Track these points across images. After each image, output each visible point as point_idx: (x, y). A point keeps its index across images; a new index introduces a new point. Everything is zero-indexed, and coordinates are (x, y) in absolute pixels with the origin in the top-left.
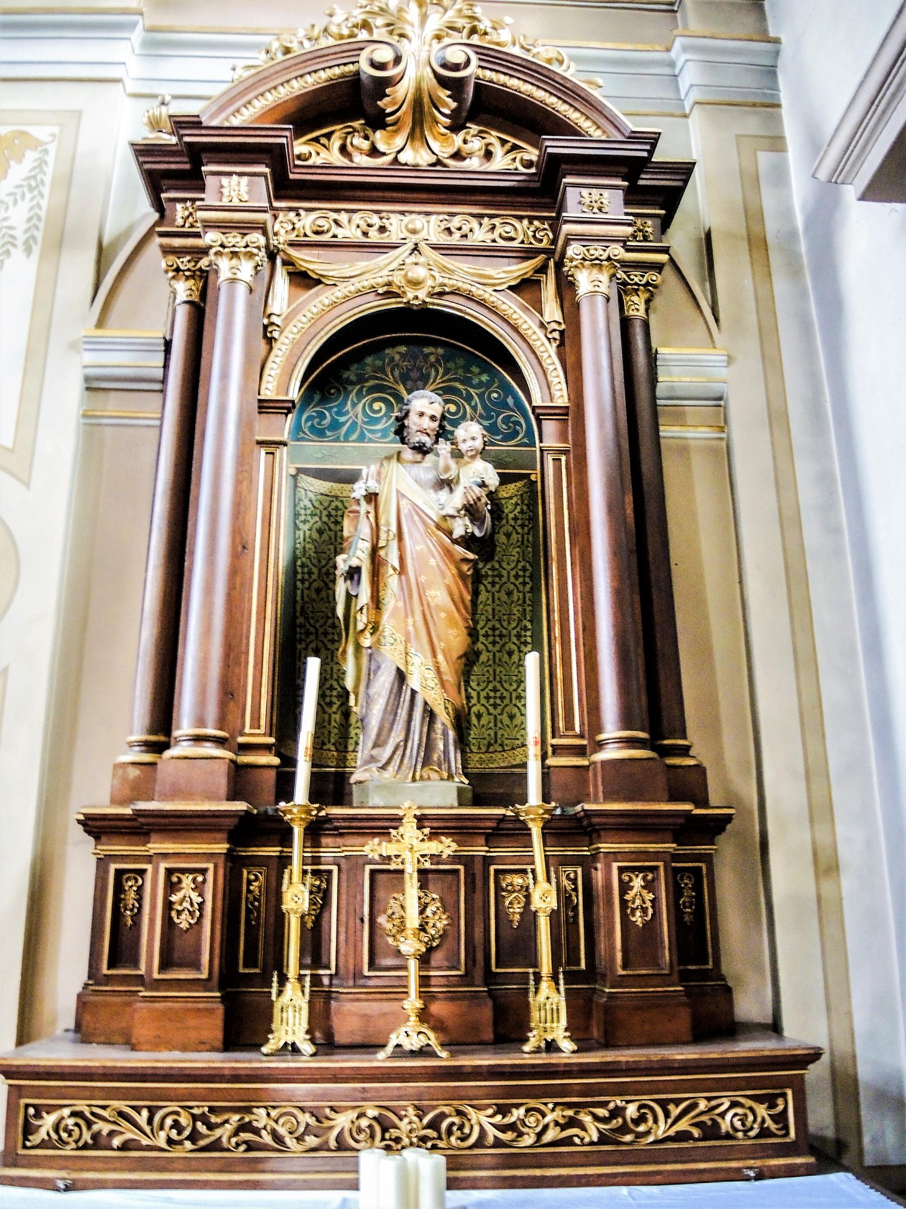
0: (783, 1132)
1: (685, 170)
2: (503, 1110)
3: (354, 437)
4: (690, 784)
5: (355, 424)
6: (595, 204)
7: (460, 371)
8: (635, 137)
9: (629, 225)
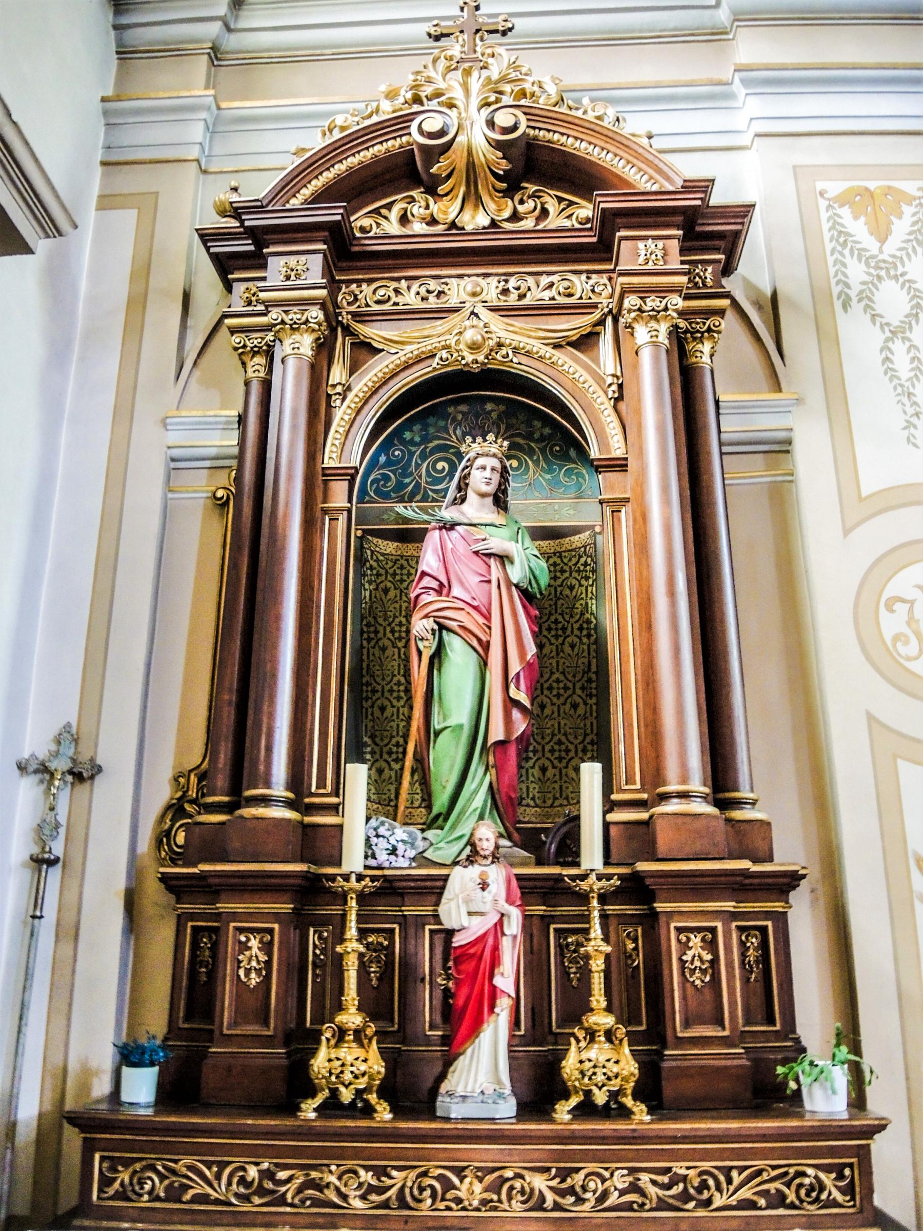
0: (852, 1203)
1: (744, 212)
2: (564, 1174)
3: (418, 498)
4: (751, 839)
5: (418, 485)
6: (648, 252)
7: (523, 426)
8: (690, 187)
9: (684, 274)
